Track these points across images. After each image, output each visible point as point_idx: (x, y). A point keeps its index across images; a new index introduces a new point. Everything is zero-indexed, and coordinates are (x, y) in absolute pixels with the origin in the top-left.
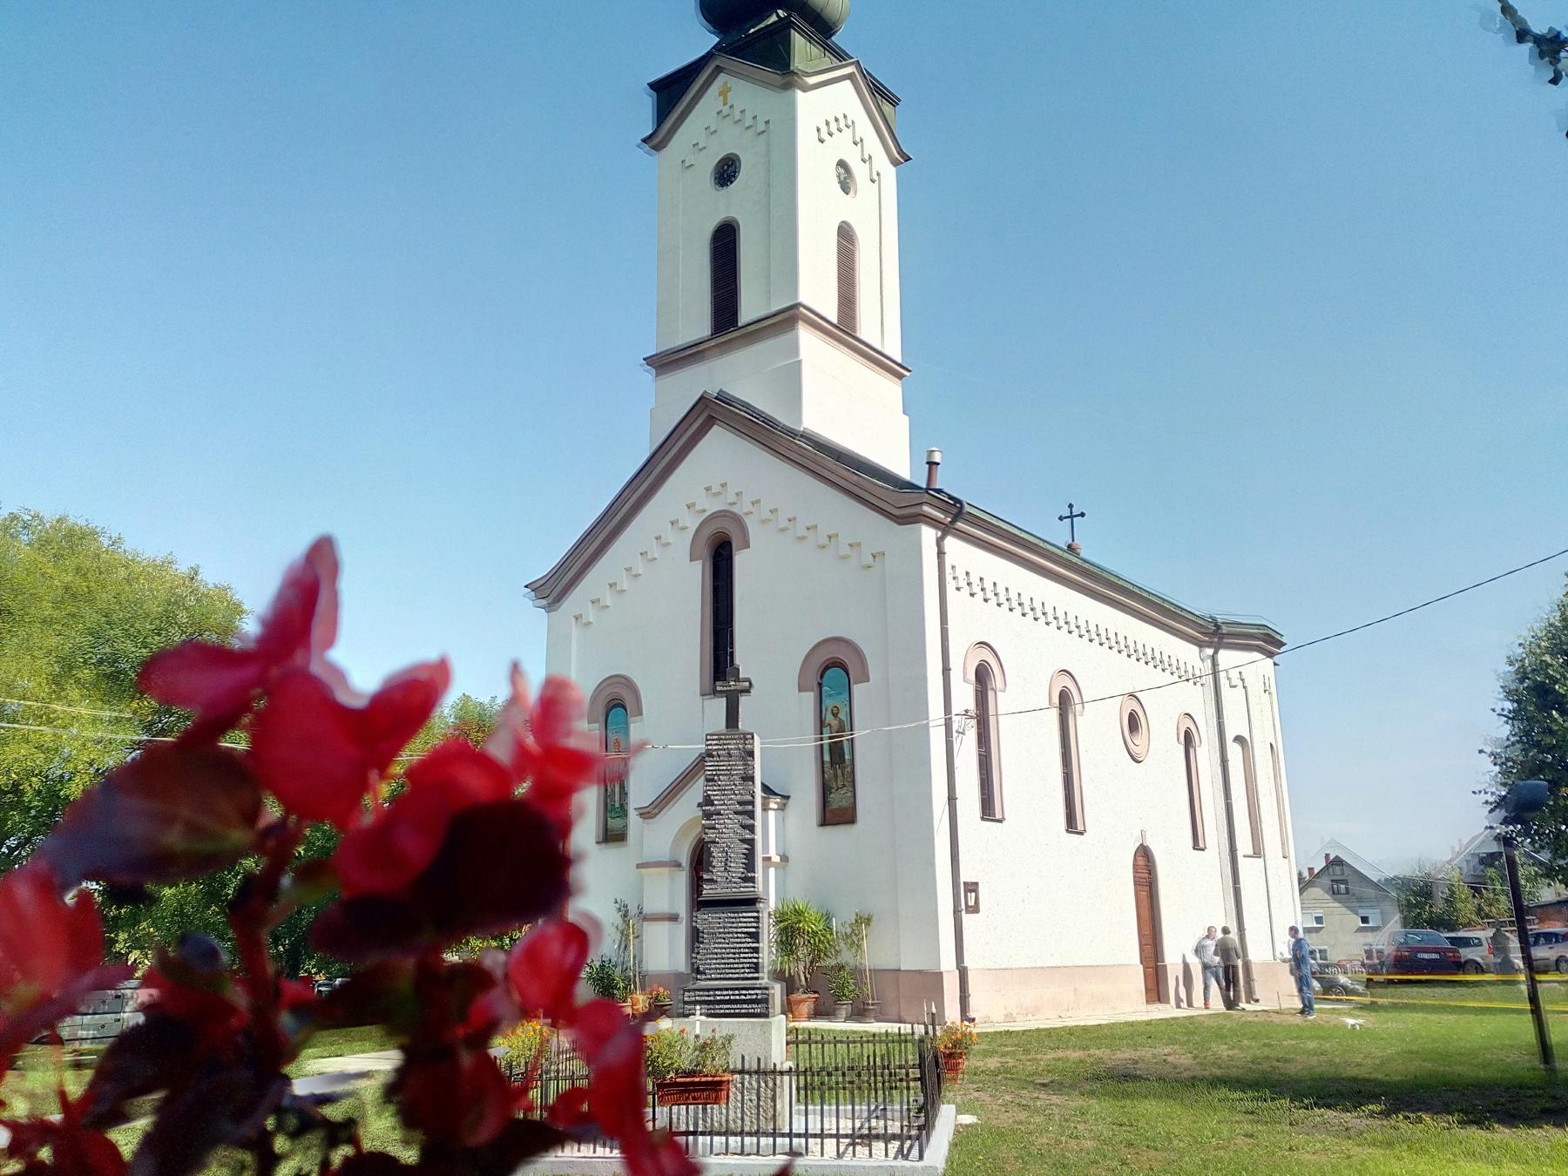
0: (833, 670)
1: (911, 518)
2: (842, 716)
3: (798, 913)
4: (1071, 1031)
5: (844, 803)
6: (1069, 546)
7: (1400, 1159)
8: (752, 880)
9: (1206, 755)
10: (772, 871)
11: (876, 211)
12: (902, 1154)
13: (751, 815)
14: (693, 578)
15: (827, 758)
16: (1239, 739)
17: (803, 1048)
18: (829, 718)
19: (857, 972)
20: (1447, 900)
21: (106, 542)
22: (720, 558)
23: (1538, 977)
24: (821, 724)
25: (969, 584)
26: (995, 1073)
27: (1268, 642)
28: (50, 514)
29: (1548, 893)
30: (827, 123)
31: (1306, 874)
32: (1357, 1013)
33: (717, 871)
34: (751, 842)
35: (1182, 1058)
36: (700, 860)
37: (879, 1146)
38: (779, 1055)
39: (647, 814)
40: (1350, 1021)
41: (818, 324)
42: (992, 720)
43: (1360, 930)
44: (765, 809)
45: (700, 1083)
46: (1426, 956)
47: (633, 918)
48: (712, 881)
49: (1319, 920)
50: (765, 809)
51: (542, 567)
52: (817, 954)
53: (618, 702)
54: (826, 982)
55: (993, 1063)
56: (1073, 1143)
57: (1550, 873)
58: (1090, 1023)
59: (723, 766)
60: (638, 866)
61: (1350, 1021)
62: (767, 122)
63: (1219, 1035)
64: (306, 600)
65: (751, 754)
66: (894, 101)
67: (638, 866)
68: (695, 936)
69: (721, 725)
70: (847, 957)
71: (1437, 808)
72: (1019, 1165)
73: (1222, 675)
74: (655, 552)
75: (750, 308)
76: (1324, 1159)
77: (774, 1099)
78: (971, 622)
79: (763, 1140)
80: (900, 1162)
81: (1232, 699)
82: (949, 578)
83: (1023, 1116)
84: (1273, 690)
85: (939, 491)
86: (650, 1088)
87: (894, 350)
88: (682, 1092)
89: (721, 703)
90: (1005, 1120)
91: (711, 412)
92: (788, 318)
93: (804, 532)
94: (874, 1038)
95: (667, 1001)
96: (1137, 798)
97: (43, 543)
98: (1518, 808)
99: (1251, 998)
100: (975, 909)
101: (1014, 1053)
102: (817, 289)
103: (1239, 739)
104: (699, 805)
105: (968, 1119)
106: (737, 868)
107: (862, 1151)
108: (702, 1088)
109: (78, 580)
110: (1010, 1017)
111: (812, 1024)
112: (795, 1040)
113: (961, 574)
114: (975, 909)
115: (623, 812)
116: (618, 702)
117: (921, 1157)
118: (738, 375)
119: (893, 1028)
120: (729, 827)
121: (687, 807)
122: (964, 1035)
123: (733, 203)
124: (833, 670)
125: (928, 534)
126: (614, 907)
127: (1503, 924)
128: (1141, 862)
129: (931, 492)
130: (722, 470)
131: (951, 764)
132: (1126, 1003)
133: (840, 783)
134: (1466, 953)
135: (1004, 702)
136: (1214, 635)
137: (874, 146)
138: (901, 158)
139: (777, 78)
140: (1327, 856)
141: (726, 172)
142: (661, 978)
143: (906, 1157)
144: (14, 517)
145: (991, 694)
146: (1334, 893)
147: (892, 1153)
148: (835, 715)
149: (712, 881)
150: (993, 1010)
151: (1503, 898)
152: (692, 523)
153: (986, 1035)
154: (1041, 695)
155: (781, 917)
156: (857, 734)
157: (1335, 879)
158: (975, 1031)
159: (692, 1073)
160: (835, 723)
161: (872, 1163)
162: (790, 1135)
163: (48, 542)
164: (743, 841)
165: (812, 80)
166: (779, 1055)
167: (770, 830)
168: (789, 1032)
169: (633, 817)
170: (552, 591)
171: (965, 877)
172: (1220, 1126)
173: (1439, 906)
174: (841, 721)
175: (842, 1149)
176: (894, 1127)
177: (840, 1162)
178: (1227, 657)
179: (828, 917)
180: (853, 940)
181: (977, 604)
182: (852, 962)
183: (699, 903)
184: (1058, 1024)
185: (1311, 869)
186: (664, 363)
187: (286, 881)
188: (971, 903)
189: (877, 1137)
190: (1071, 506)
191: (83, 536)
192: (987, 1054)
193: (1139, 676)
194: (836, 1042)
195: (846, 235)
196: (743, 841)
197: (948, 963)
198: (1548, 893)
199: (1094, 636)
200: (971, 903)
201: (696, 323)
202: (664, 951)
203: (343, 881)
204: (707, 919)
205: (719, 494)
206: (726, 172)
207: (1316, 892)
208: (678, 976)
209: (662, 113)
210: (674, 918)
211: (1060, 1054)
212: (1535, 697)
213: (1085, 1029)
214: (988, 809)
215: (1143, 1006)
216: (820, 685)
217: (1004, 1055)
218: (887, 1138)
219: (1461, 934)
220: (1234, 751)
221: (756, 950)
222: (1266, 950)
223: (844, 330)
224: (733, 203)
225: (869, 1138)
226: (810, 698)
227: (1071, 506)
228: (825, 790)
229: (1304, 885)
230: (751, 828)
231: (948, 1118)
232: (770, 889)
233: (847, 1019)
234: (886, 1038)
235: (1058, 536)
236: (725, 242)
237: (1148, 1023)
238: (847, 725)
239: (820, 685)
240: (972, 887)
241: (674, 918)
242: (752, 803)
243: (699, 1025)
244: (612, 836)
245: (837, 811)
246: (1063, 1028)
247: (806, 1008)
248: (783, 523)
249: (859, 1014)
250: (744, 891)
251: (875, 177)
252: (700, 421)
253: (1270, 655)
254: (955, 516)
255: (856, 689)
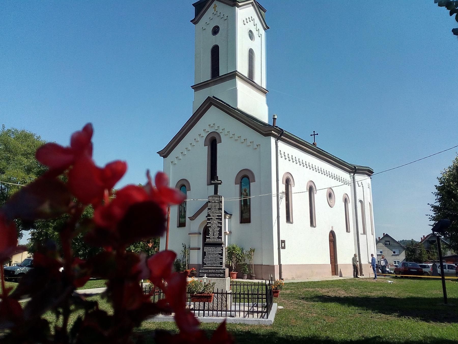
0: (245, 178)
1: (268, 135)
2: (247, 191)
3: (234, 248)
4: (310, 283)
5: (247, 217)
6: (313, 144)
7: (402, 320)
8: (221, 238)
9: (350, 206)
10: (227, 236)
11: (259, 45)
12: (262, 317)
13: (221, 219)
14: (205, 151)
15: (242, 204)
16: (361, 201)
17: (235, 287)
18: (243, 192)
19: (249, 266)
20: (419, 254)
21: (36, 138)
22: (213, 143)
23: (446, 278)
24: (241, 194)
25: (285, 156)
26: (288, 295)
27: (369, 172)
28: (20, 129)
29: (449, 253)
30: (246, 19)
31: (378, 239)
32: (391, 279)
33: (211, 235)
34: (221, 227)
35: (342, 294)
36: (206, 232)
37: (255, 315)
38: (228, 289)
39: (192, 219)
40: (390, 282)
41: (242, 78)
42: (290, 193)
43: (393, 255)
44: (225, 218)
45: (204, 296)
46: (413, 270)
47: (187, 249)
48: (209, 238)
49: (381, 252)
50: (225, 218)
51: (162, 147)
52: (238, 260)
53: (184, 185)
54: (241, 269)
55: (288, 292)
56: (310, 315)
57: (450, 247)
58: (316, 280)
59: (212, 206)
60: (189, 234)
61: (390, 282)
62: (227, 16)
63: (352, 285)
64: (83, 140)
65: (221, 202)
66: (265, 11)
67: (189, 234)
68: (204, 254)
69: (213, 194)
70: (247, 261)
71: (417, 225)
72: (295, 321)
73: (356, 183)
74: (194, 143)
75: (222, 72)
76: (381, 320)
77: (226, 301)
78: (285, 167)
79: (223, 312)
80: (261, 319)
81: (359, 189)
82: (279, 154)
83: (296, 307)
84: (371, 187)
85: (277, 127)
86: (189, 297)
87: (264, 86)
88: (198, 298)
89: (213, 186)
90: (291, 308)
91: (211, 102)
92: (233, 75)
93: (237, 138)
94: (255, 284)
95: (195, 272)
96: (331, 217)
97: (17, 138)
98: (439, 226)
99: (361, 274)
100: (284, 248)
101: (294, 289)
102: (242, 67)
103: (361, 201)
104: (207, 217)
105: (281, 307)
106: (217, 235)
107: (251, 316)
108: (204, 297)
109: (28, 149)
110: (293, 278)
111: (237, 280)
112: (232, 284)
113: (282, 153)
114: (284, 248)
115: (184, 217)
116: (184, 185)
117: (267, 318)
118: (219, 91)
119: (260, 281)
120: (215, 223)
121: (203, 217)
122: (280, 284)
123: (217, 40)
124: (245, 178)
125: (273, 140)
126: (182, 246)
127: (436, 262)
128: (331, 235)
129: (274, 127)
130: (213, 119)
131: (278, 207)
132: (328, 276)
133: (246, 211)
134: (424, 270)
135: (294, 189)
136: (354, 170)
137: (260, 26)
138: (266, 28)
139: (232, 3)
140: (384, 234)
141: (216, 31)
142: (194, 266)
143: (263, 318)
144: (9, 131)
145: (289, 186)
146: (386, 245)
147: (259, 317)
148: (245, 191)
149: (209, 238)
150: (288, 277)
151: (436, 254)
152: (205, 135)
153: (286, 283)
154: (305, 189)
155: (229, 249)
156: (252, 197)
157: (386, 241)
158: (283, 282)
159: (201, 293)
160: (245, 193)
161: (254, 319)
162: (231, 311)
163: (19, 138)
164: (218, 227)
165: (240, 4)
166: (228, 289)
167: (226, 224)
168: (231, 282)
169: (187, 220)
170: (165, 153)
171: (281, 239)
172: (353, 311)
173: (417, 256)
174: (247, 193)
175: (245, 315)
176: (260, 309)
177: (245, 319)
178: (358, 177)
179: (242, 250)
180: (250, 256)
181: (287, 161)
182: (248, 263)
183: (205, 244)
184: (307, 281)
185: (379, 238)
186: (197, 87)
187: (77, 225)
188: (283, 246)
189: (255, 312)
190: (314, 132)
191: (30, 136)
192: (286, 289)
193: (332, 183)
194: (244, 285)
195: (251, 52)
196: (218, 227)
197: (276, 263)
198: (449, 253)
199: (320, 171)
200: (283, 246)
201: (207, 76)
202: (195, 258)
203: (90, 219)
204: (207, 249)
205: (213, 127)
206: (216, 31)
207: (381, 244)
208: (199, 265)
209: (197, 13)
210: (199, 249)
211: (307, 289)
212: (446, 192)
213: (314, 282)
214: (288, 219)
215: (331, 276)
216: (241, 183)
217: (292, 289)
218: (258, 312)
219: (423, 264)
220: (359, 204)
221: (222, 258)
222: (365, 261)
223: (250, 80)
224: (217, 40)
225: (253, 312)
226: (238, 186)
227: (314, 132)
228: (242, 213)
229: (377, 242)
230: (221, 223)
231: (275, 307)
232: (226, 241)
233: (247, 279)
234: (258, 284)
235: (310, 141)
236: (215, 51)
237: (332, 281)
238: (249, 194)
239: (241, 183)
240: (283, 242)
241: (199, 249)
242: (221, 216)
243: (205, 279)
244: (182, 224)
245: (245, 218)
246: (308, 282)
247: (235, 275)
248: (231, 136)
249: (250, 277)
250: (218, 241)
251: (260, 35)
252: (208, 104)
253: (369, 175)
254: (281, 135)
255: (252, 184)
